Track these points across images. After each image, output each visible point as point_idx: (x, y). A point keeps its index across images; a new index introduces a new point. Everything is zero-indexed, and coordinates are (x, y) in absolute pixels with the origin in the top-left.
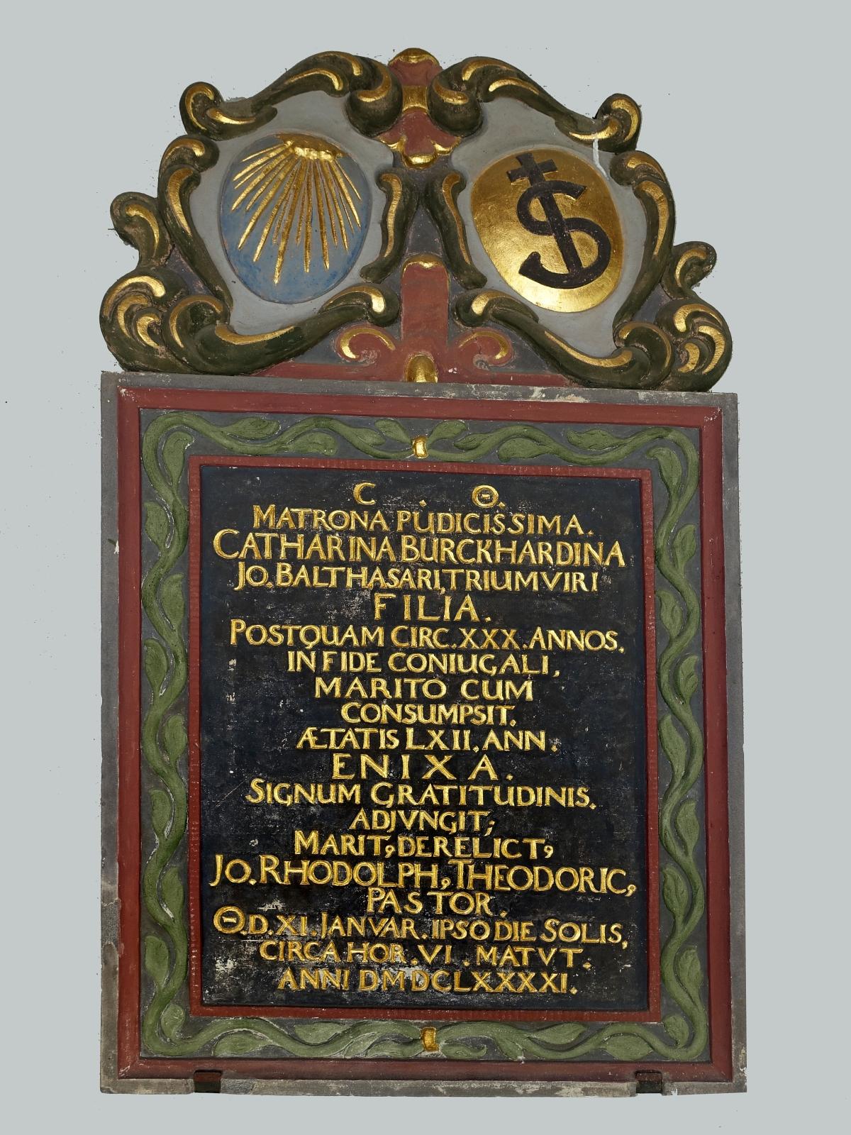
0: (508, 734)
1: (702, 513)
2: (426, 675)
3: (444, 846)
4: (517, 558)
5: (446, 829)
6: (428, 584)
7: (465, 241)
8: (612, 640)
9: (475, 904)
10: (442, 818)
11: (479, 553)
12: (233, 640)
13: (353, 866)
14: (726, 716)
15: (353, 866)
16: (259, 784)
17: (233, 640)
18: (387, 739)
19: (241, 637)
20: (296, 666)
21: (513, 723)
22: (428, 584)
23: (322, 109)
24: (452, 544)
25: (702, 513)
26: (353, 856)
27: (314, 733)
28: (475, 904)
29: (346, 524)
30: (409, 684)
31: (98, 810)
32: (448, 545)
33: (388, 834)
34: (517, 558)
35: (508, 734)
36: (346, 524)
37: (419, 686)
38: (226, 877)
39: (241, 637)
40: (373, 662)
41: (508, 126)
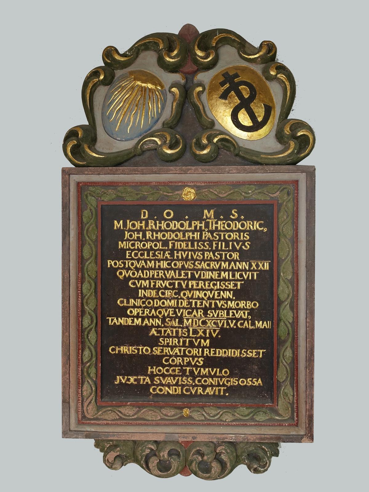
0: (238, 263)
1: (187, 434)
3: (176, 342)
4: (216, 370)
5: (163, 296)
7: (210, 173)
10: (192, 353)
12: (109, 266)
17: (109, 266)
19: (111, 265)
20: (141, 295)
21: (234, 298)
23: (148, 60)
25: (187, 434)
26: (202, 394)
27: (155, 330)
31: (61, 326)
34: (216, 370)
35: (238, 263)
38: (111, 365)
39: (111, 265)
41: (229, 58)
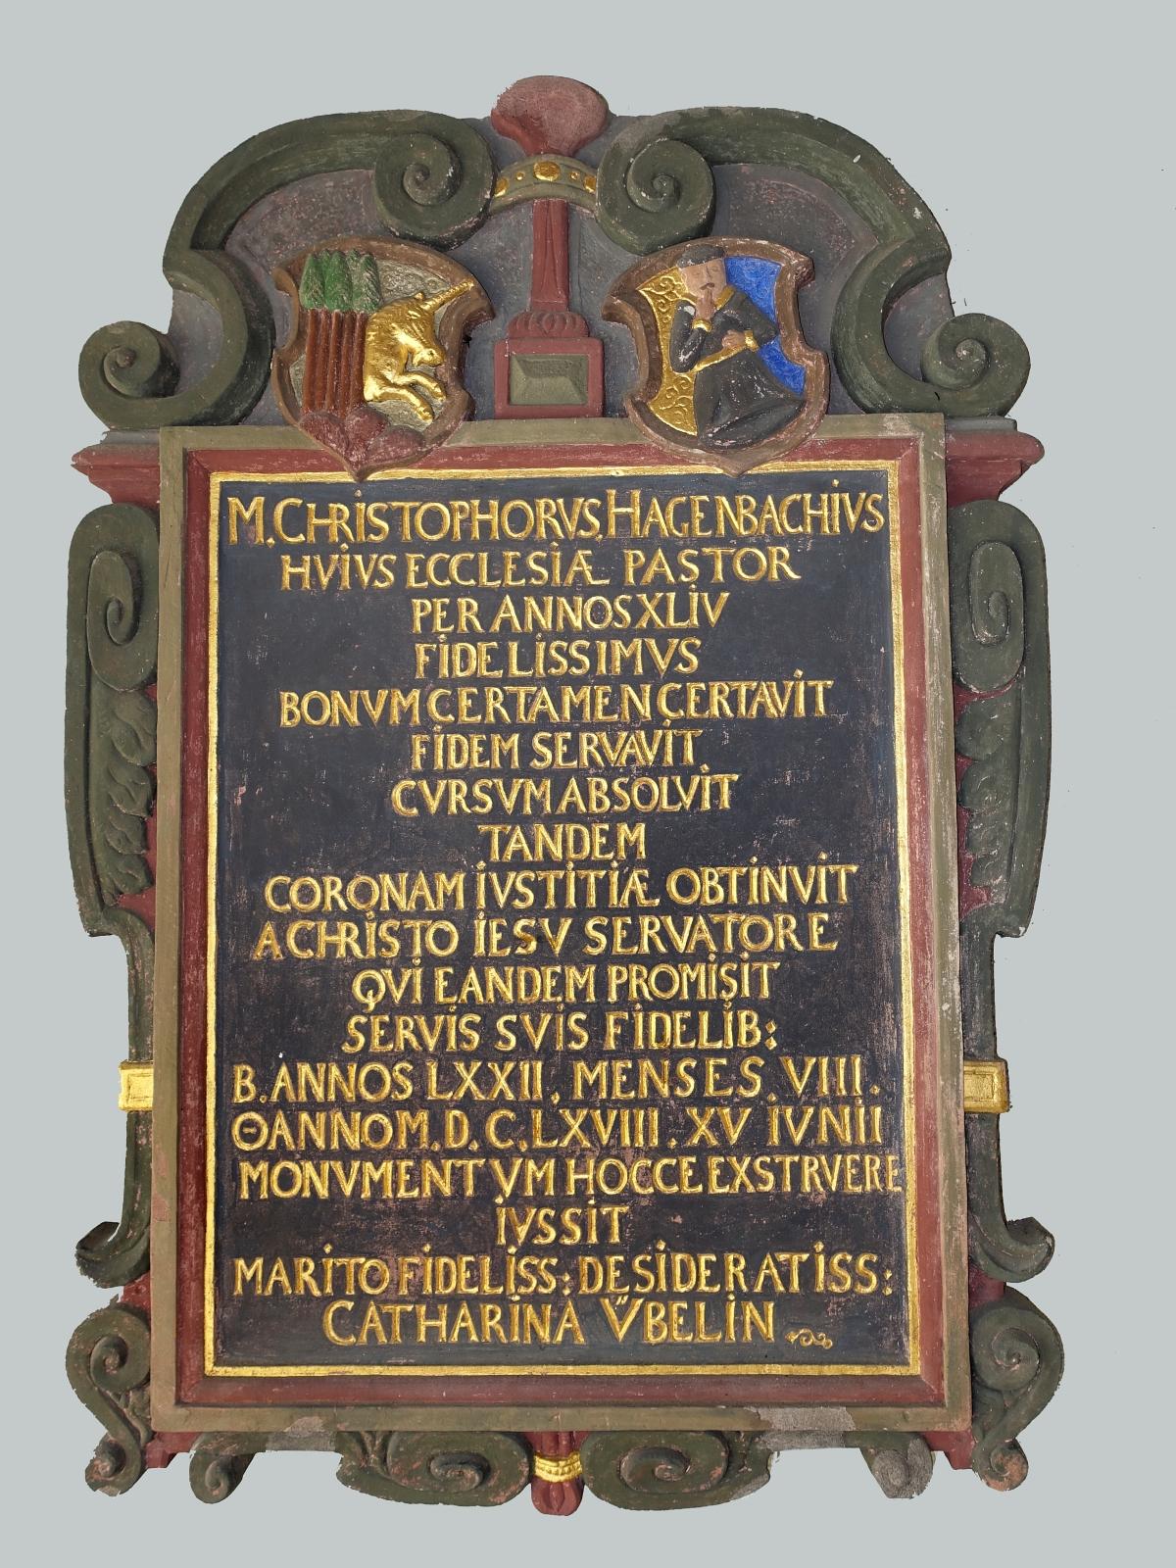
2: (448, 545)
6: (357, 950)
8: (390, 939)
9: (323, 892)
11: (491, 710)
13: (629, 1188)
14: (570, 417)
15: (629, 1188)
16: (402, 1091)
18: (549, 567)
22: (357, 950)
24: (645, 971)
28: (323, 892)
29: (529, 529)
30: (586, 879)
32: (747, 504)
33: (677, 577)
36: (529, 529)
37: (728, 561)
40: (481, 749)
